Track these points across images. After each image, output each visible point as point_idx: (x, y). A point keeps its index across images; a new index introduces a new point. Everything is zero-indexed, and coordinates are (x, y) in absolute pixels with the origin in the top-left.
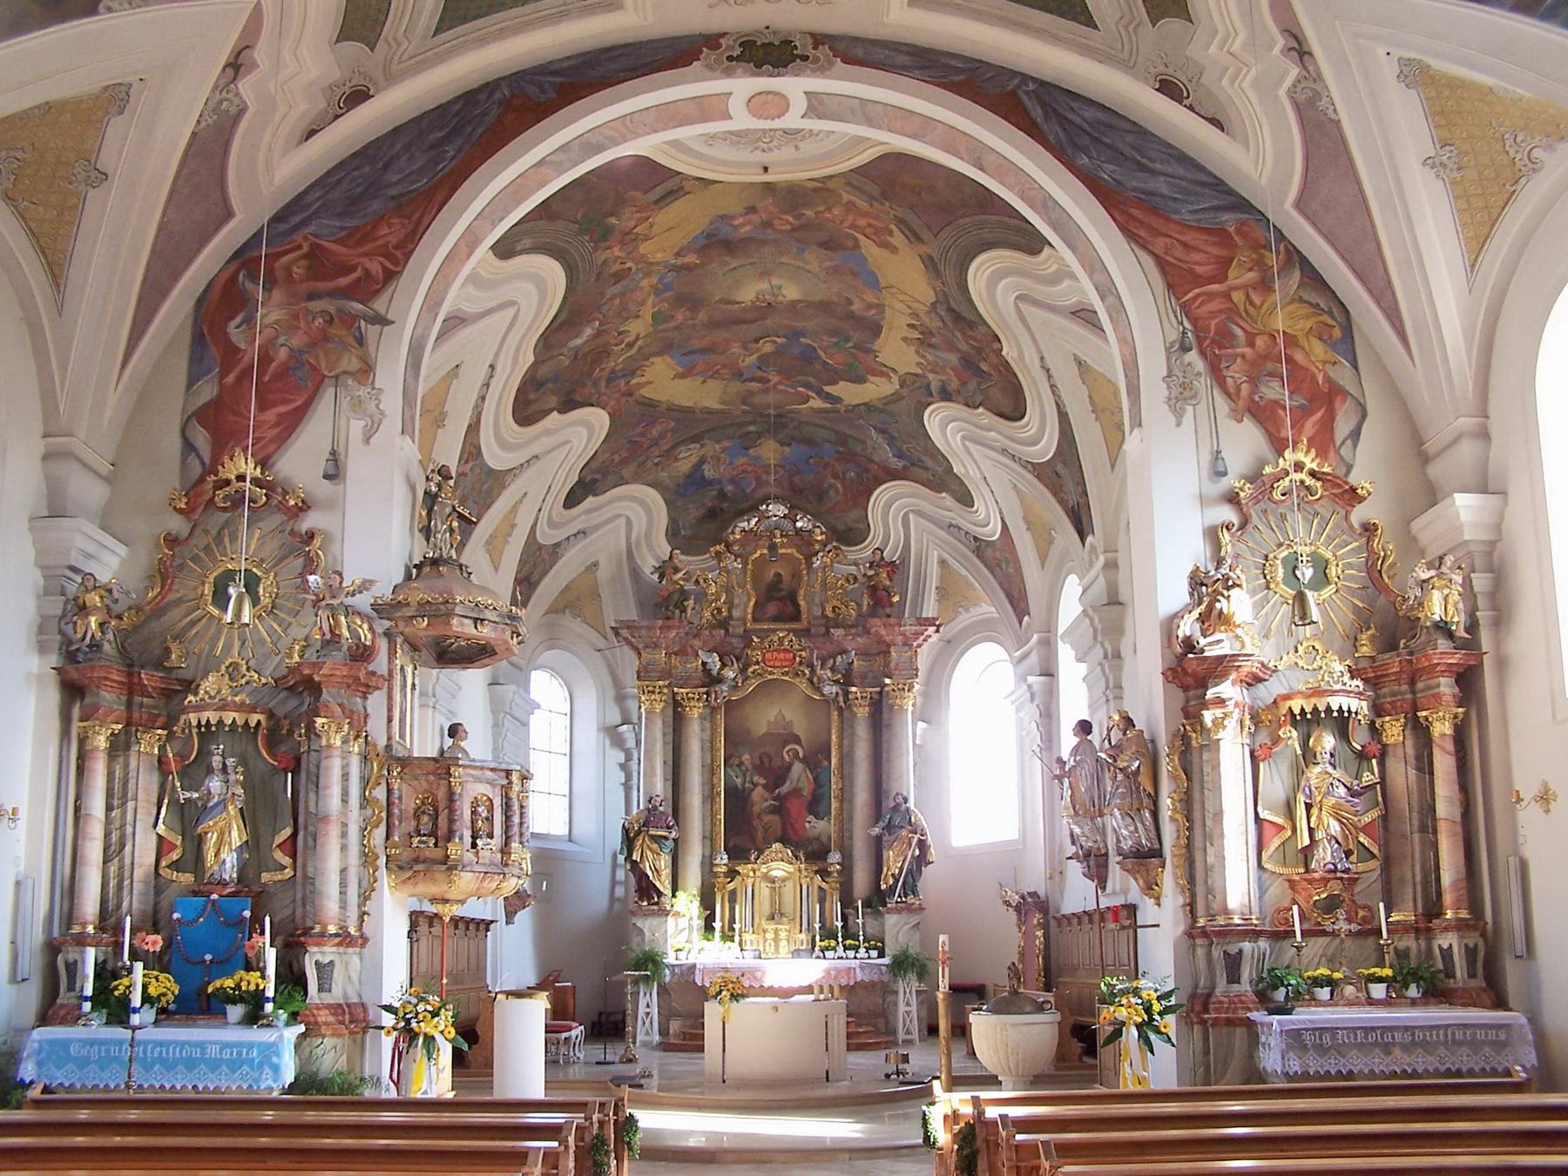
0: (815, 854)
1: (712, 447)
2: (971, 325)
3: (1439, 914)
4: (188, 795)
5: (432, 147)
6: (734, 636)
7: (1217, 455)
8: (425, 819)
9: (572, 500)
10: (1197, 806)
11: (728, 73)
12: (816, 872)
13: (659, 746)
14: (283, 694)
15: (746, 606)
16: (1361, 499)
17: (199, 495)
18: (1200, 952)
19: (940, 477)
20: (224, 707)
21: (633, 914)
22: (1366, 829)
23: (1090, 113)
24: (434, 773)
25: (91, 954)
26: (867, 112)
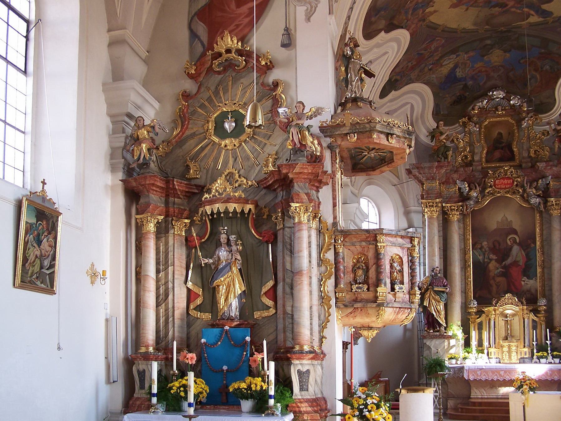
0: (530, 300)
4: (206, 261)
8: (360, 272)
12: (531, 311)
13: (436, 238)
14: (264, 191)
15: (481, 153)
17: (203, 64)
20: (228, 200)
21: (424, 337)
24: (365, 240)
25: (155, 366)
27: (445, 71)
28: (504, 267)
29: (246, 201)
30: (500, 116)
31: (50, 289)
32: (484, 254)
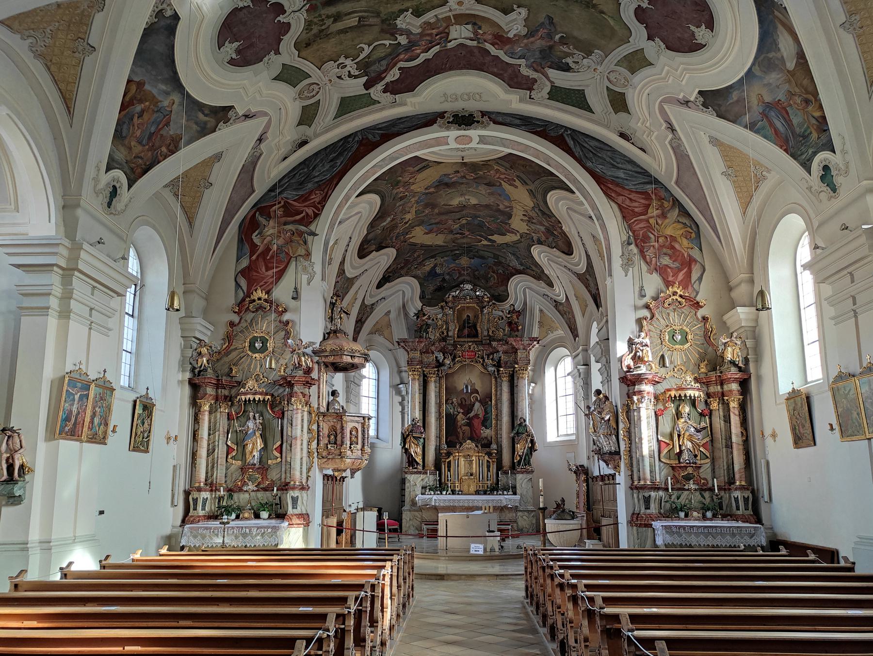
0: (485, 445)
1: (439, 260)
2: (549, 217)
3: (734, 483)
5: (331, 161)
7: (642, 288)
8: (332, 437)
9: (379, 286)
10: (633, 434)
11: (448, 129)
13: (417, 395)
16: (701, 307)
18: (635, 495)
19: (540, 275)
20: (255, 394)
22: (704, 446)
23: (593, 143)
26: (503, 142)
27: (427, 268)
29: (267, 394)
30: (468, 303)
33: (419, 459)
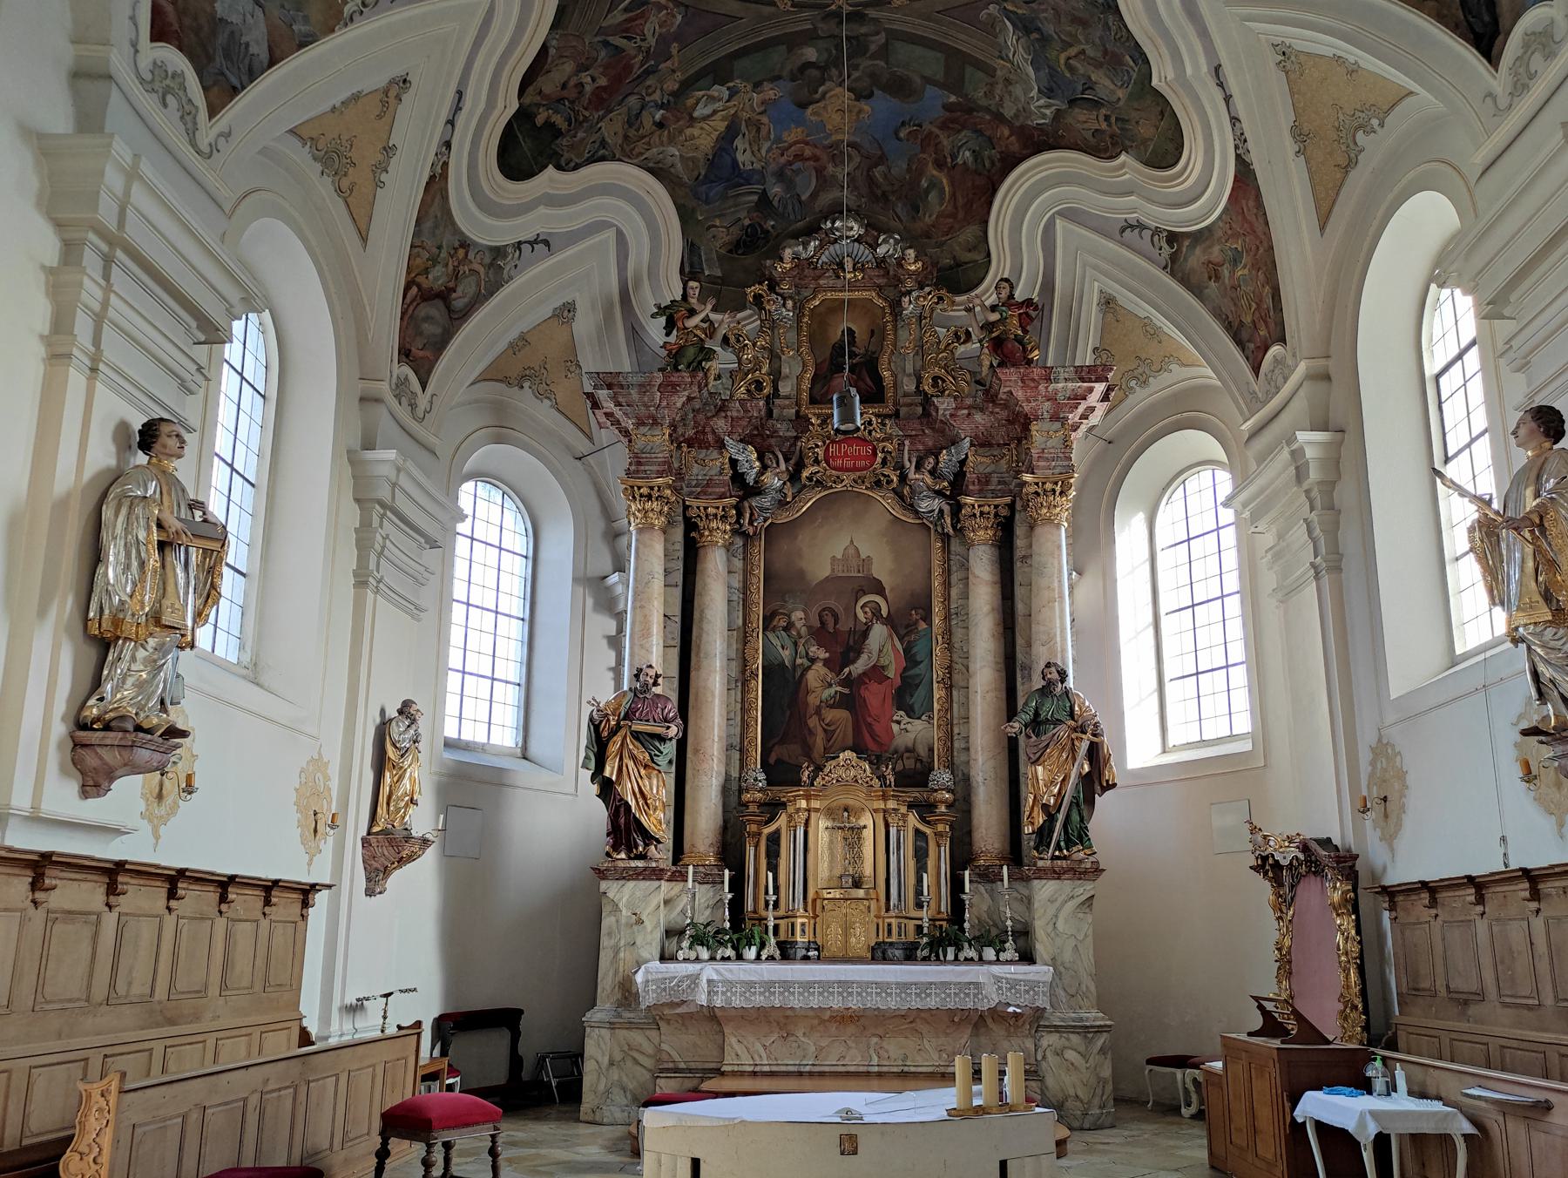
0: (912, 776)
6: (781, 419)
13: (658, 584)
27: (704, 138)
28: (847, 682)
30: (853, 286)
31: (521, 1012)
32: (796, 644)
33: (657, 821)
